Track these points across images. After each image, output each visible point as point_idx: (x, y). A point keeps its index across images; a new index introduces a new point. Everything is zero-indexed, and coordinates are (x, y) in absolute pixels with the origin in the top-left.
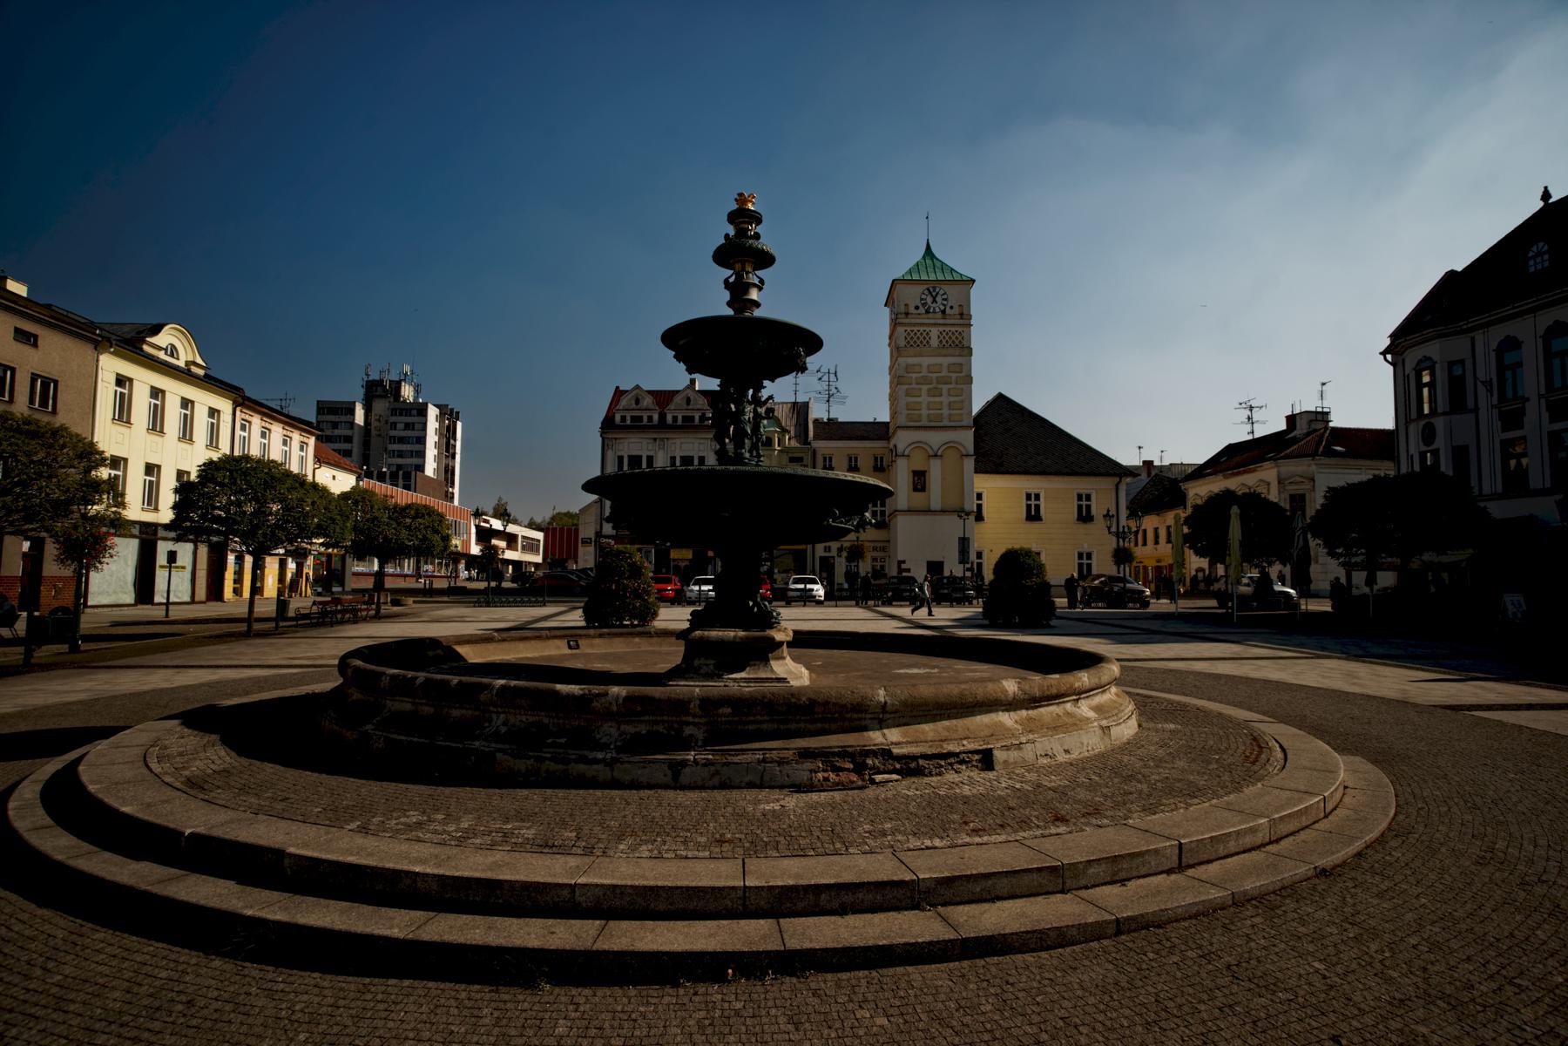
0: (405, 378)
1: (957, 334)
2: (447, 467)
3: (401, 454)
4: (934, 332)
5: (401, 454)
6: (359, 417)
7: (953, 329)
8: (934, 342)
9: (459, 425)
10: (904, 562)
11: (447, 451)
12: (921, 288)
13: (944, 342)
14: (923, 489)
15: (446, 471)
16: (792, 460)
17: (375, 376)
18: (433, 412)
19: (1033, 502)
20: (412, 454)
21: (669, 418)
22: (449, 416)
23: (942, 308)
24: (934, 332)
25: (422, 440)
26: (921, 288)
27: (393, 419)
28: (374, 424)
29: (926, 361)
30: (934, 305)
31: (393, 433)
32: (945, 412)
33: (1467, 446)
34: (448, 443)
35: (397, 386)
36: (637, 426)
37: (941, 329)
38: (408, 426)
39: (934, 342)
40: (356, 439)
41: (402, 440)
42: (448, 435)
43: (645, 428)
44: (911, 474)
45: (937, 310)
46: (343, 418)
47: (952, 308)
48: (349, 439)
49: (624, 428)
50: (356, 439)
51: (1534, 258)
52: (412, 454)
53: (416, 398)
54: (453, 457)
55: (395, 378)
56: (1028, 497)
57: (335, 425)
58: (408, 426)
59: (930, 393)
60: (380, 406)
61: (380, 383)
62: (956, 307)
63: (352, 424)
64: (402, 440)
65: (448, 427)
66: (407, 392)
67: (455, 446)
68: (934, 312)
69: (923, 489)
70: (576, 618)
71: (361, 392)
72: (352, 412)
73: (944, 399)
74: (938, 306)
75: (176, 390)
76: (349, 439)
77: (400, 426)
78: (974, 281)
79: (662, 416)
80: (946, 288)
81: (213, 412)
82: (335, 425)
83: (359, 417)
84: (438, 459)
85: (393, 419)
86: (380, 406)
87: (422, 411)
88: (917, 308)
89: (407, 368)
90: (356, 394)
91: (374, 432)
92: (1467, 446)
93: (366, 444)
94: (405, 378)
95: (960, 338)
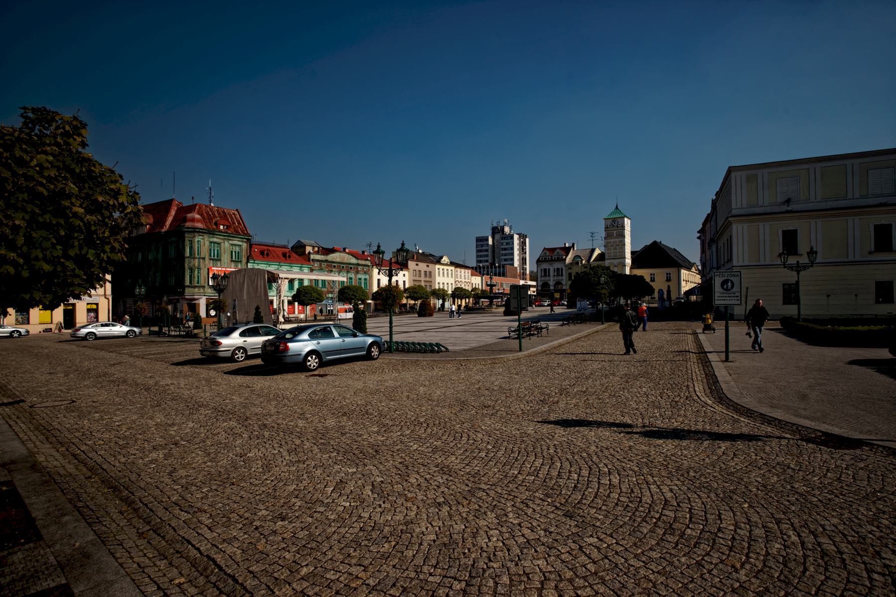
0: (505, 224)
2: (523, 258)
3: (506, 255)
4: (615, 232)
5: (506, 255)
6: (490, 242)
8: (615, 235)
9: (527, 240)
11: (523, 251)
12: (611, 220)
15: (523, 259)
16: (585, 268)
17: (495, 225)
18: (516, 237)
19: (652, 276)
20: (509, 254)
21: (553, 258)
22: (523, 237)
24: (615, 232)
25: (512, 249)
26: (611, 220)
27: (502, 241)
28: (496, 243)
29: (612, 240)
31: (502, 247)
32: (618, 254)
33: (891, 225)
34: (523, 248)
35: (503, 228)
36: (545, 261)
38: (507, 244)
39: (615, 235)
40: (490, 250)
41: (505, 249)
42: (523, 244)
43: (547, 261)
46: (485, 243)
48: (487, 251)
49: (542, 261)
50: (490, 250)
52: (509, 254)
53: (510, 231)
54: (525, 253)
55: (502, 224)
56: (651, 275)
57: (482, 246)
58: (507, 244)
59: (614, 249)
60: (497, 236)
61: (496, 228)
63: (488, 245)
64: (505, 249)
65: (523, 242)
66: (507, 230)
67: (526, 249)
70: (417, 315)
71: (490, 232)
72: (487, 240)
73: (618, 250)
74: (616, 225)
75: (445, 268)
76: (487, 251)
77: (505, 244)
79: (552, 257)
80: (618, 219)
81: (452, 270)
82: (482, 246)
83: (490, 242)
84: (519, 255)
85: (502, 241)
86: (497, 236)
87: (512, 237)
89: (506, 221)
90: (488, 233)
91: (496, 247)
92: (891, 225)
93: (494, 252)
94: (505, 224)
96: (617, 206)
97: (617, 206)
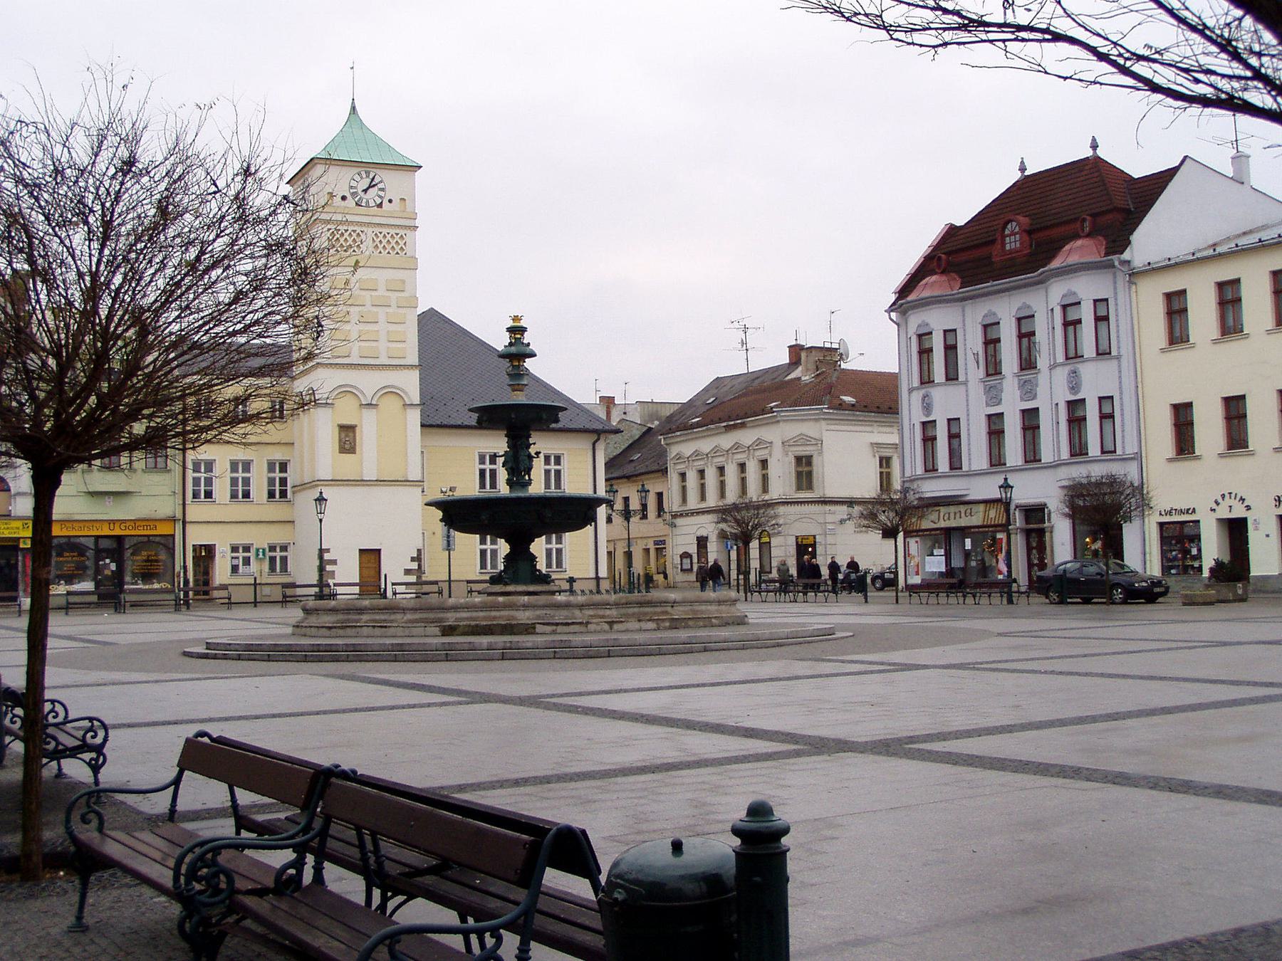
1: (397, 238)
7: (393, 231)
10: (328, 550)
13: (381, 248)
14: (352, 450)
23: (379, 201)
30: (362, 194)
37: (377, 230)
44: (337, 429)
45: (371, 202)
47: (390, 201)
51: (1010, 236)
62: (396, 201)
68: (368, 206)
69: (352, 450)
78: (421, 167)
88: (344, 198)
95: (402, 243)
96: (354, 108)
97: (354, 108)
